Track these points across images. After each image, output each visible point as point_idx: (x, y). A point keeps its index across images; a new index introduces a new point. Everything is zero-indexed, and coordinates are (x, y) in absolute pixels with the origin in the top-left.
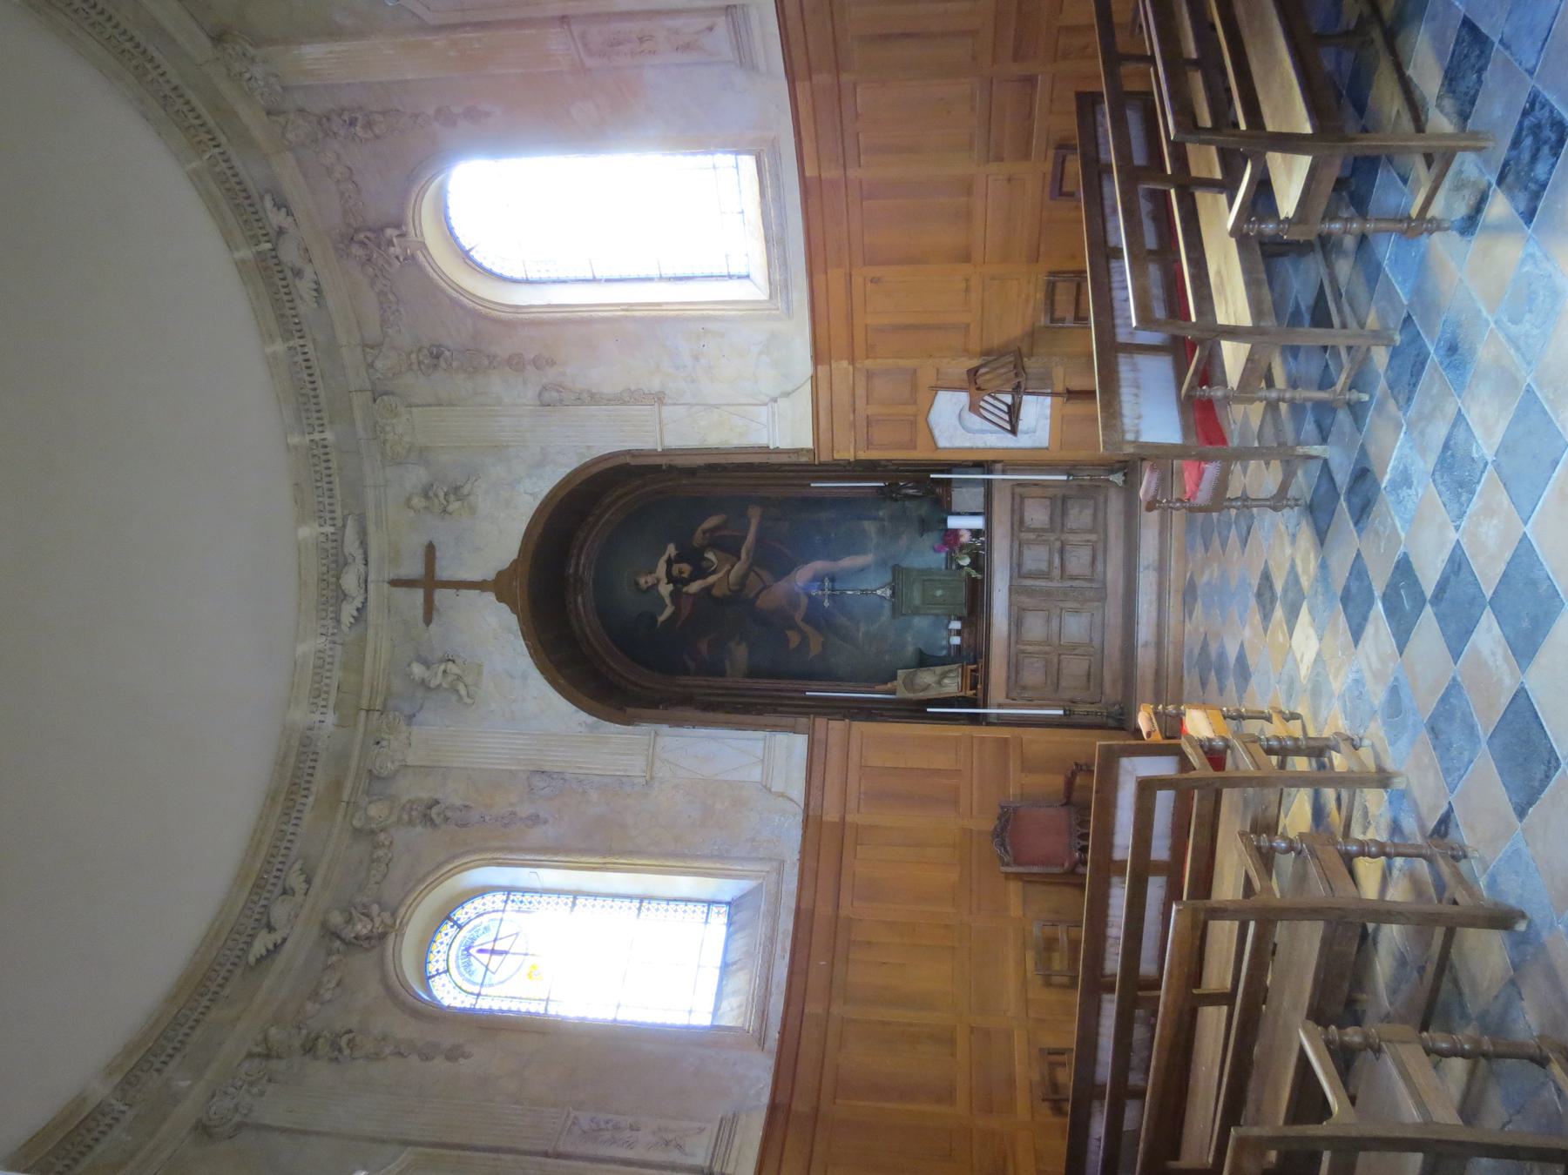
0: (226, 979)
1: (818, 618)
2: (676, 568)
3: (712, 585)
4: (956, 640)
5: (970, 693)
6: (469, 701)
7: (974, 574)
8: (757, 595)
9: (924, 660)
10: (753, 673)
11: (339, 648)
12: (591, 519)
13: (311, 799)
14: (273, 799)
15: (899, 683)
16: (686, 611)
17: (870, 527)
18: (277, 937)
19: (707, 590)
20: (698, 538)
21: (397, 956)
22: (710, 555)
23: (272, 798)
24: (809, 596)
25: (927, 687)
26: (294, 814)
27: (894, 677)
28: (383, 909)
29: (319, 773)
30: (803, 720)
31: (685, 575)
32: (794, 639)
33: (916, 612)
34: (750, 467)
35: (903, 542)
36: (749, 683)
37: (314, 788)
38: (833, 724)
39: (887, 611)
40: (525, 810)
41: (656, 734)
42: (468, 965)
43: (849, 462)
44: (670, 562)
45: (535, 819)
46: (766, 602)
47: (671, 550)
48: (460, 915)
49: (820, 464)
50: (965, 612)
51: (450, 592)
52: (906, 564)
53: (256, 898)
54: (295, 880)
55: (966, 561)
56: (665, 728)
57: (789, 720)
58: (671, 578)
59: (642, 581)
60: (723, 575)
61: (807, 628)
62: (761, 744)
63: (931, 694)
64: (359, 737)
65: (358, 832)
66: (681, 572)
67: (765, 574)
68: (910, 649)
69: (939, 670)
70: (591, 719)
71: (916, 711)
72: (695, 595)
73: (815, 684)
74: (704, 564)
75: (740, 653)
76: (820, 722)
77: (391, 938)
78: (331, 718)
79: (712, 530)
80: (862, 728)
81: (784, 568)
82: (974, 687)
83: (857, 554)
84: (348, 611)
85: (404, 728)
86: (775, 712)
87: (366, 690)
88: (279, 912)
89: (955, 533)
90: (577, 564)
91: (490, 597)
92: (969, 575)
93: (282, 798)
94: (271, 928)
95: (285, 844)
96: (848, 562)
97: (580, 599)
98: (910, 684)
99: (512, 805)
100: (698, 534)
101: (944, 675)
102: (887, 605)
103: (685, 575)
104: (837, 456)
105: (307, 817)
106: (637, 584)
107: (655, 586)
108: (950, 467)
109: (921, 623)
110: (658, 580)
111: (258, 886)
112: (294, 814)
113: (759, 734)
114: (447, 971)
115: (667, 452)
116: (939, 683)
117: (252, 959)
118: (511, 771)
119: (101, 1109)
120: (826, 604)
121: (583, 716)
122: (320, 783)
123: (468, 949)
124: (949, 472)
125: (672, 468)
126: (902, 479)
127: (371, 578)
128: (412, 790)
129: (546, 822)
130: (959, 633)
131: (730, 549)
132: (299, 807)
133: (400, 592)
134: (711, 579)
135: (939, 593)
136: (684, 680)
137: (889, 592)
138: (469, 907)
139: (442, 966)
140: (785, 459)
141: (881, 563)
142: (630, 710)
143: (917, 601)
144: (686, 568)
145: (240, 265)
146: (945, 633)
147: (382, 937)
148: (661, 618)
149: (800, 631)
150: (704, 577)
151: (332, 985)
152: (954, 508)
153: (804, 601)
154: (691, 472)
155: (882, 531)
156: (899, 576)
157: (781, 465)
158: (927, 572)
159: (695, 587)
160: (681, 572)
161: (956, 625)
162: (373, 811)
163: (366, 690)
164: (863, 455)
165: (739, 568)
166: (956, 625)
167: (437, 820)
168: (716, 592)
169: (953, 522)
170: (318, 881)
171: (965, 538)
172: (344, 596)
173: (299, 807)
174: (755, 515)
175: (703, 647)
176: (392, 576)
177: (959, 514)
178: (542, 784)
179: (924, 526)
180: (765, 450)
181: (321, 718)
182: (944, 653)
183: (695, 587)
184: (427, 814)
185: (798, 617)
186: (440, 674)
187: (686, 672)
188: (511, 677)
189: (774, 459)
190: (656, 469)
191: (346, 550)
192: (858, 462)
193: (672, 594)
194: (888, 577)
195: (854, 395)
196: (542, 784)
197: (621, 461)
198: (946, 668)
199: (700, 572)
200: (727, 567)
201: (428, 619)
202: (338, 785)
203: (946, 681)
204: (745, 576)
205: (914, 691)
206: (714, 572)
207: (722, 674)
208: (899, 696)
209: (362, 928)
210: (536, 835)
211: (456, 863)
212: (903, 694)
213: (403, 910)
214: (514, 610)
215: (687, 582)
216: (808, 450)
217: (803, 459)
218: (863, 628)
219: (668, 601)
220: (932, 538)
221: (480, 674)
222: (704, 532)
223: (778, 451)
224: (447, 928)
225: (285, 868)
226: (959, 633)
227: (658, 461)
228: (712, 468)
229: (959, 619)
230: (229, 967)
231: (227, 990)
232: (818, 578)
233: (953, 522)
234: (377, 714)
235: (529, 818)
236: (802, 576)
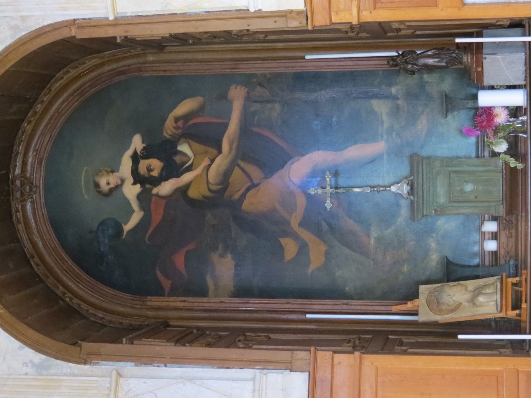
1: (319, 222)
2: (143, 165)
3: (187, 186)
4: (491, 246)
5: (512, 314)
7: (513, 163)
8: (244, 196)
9: (453, 272)
10: (243, 291)
12: (39, 107)
15: (421, 302)
16: (157, 217)
17: (381, 107)
19: (183, 190)
20: (169, 127)
22: (184, 148)
24: (308, 196)
25: (458, 306)
27: (414, 295)
30: (302, 355)
31: (155, 173)
32: (290, 248)
33: (441, 211)
34: (227, 37)
35: (423, 124)
36: (238, 303)
38: (338, 357)
39: (405, 212)
41: (119, 375)
43: (352, 27)
44: (135, 158)
46: (254, 203)
47: (137, 143)
49: (315, 31)
50: (501, 211)
52: (425, 152)
55: (502, 147)
56: (129, 368)
57: (284, 355)
58: (137, 178)
59: (103, 182)
60: (201, 171)
61: (305, 235)
62: (249, 386)
63: (464, 315)
66: (149, 170)
67: (251, 169)
68: (434, 259)
69: (471, 284)
70: (38, 357)
71: (443, 337)
72: (167, 198)
73: (317, 304)
74: (178, 159)
75: (224, 270)
76: (324, 356)
79: (186, 117)
80: (377, 363)
81: (272, 161)
82: (516, 306)
83: (365, 141)
86: (269, 341)
89: (489, 111)
90: (24, 164)
92: (506, 164)
96: (354, 152)
97: (29, 207)
98: (435, 304)
100: (169, 123)
101: (478, 292)
102: (404, 204)
103: (155, 173)
104: (335, 19)
106: (97, 185)
107: (118, 187)
108: (480, 28)
109: (447, 224)
110: (123, 181)
113: (248, 373)
115: (118, 22)
116: (473, 301)
119: (189, 343)
120: (328, 205)
121: (30, 354)
124: (479, 35)
125: (130, 42)
126: (420, 46)
130: (495, 236)
131: (208, 137)
134: (187, 177)
135: (469, 188)
136: (154, 301)
137: (406, 189)
140: (269, 25)
141: (396, 152)
142: (87, 346)
143: (442, 200)
144: (156, 165)
145: (115, 38)
146: (477, 237)
148: (127, 227)
149: (295, 236)
150: (178, 176)
152: (487, 82)
153: (301, 201)
154: (158, 45)
155: (396, 111)
156: (419, 168)
157: (267, 33)
158: (450, 161)
159: (166, 188)
160: (149, 170)
161: (491, 227)
164: (372, 16)
165: (221, 163)
166: (491, 227)
168: (192, 193)
169: (485, 99)
171: (501, 118)
174: (237, 95)
175: (179, 260)
177: (492, 88)
179: (448, 104)
180: (243, 14)
182: (477, 261)
183: (166, 188)
185: (294, 223)
187: (159, 292)
189: (256, 25)
190: (108, 43)
192: (363, 27)
193: (139, 197)
194: (404, 170)
197: (65, 34)
198: (480, 282)
199: (172, 170)
200: (206, 162)
203: (481, 299)
204: (226, 175)
205: (440, 312)
206: (190, 169)
207: (203, 293)
208: (420, 318)
212: (426, 315)
215: (157, 182)
216: (299, 13)
217: (294, 24)
218: (374, 233)
219: (135, 205)
220: (459, 119)
222: (177, 120)
223: (260, 15)
226: (495, 236)
227: (110, 32)
228: (181, 40)
229: (494, 218)
232: (317, 173)
233: (485, 99)
236: (298, 171)
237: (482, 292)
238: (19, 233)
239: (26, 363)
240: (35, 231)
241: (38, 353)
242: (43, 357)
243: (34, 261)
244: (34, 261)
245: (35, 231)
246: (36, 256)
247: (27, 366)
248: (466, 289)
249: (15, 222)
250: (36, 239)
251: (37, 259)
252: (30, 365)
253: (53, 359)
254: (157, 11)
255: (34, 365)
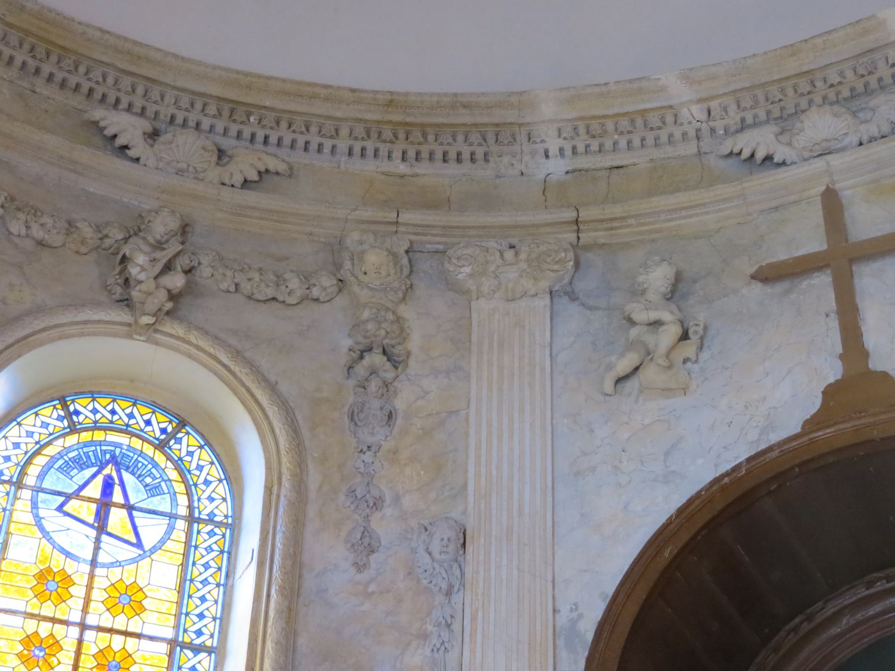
0: (63, 84)
6: (609, 386)
11: (690, 148)
13: (402, 168)
14: (390, 103)
18: (139, 148)
21: (86, 329)
23: (392, 102)
26: (370, 145)
28: (173, 297)
29: (452, 169)
37: (423, 168)
40: (385, 526)
42: (80, 463)
45: (365, 546)
48: (188, 442)
51: (830, 300)
53: (212, 110)
54: (246, 163)
64: (523, 218)
65: (335, 248)
77: (125, 316)
78: (557, 167)
84: (761, 141)
85: (544, 284)
87: (617, 210)
88: (185, 146)
91: (832, 371)
93: (397, 117)
94: (154, 135)
95: (315, 140)
99: (397, 499)
105: (369, 166)
111: (233, 109)
112: (370, 145)
114: (73, 429)
117: (98, 114)
118: (465, 487)
122: (433, 175)
123: (114, 460)
127: (835, 160)
128: (423, 325)
129: (360, 567)
132: (384, 149)
133: (816, 215)
138: (103, 405)
139: (85, 417)
147: (126, 302)
151: (37, 232)
162: (374, 259)
163: (617, 210)
167: (361, 370)
170: (250, 197)
172: (786, 121)
173: (384, 149)
176: (846, 195)
178: (436, 546)
181: (553, 151)
184: (381, 353)
186: (653, 315)
188: (667, 454)
191: (879, 100)
195: (552, 380)
196: (436, 546)
201: (768, 275)
202: (433, 202)
209: (141, 264)
210: (329, 552)
211: (273, 412)
213: (180, 330)
214: (812, 424)
221: (667, 392)
224: (160, 422)
225: (271, 149)
230: (86, 86)
231: (44, 89)
234: (572, 237)
235: (366, 532)
237: (160, 328)
238: (848, 590)
239: (577, 609)
240: (859, 616)
241: (595, 627)
242: (590, 636)
243: (802, 622)
244: (802, 622)
245: (859, 616)
246: (812, 625)
247: (571, 610)
248: (169, 291)
249: (867, 578)
250: (845, 621)
251: (806, 627)
252: (574, 615)
253: (586, 654)
254: (792, 50)
255: (574, 622)
